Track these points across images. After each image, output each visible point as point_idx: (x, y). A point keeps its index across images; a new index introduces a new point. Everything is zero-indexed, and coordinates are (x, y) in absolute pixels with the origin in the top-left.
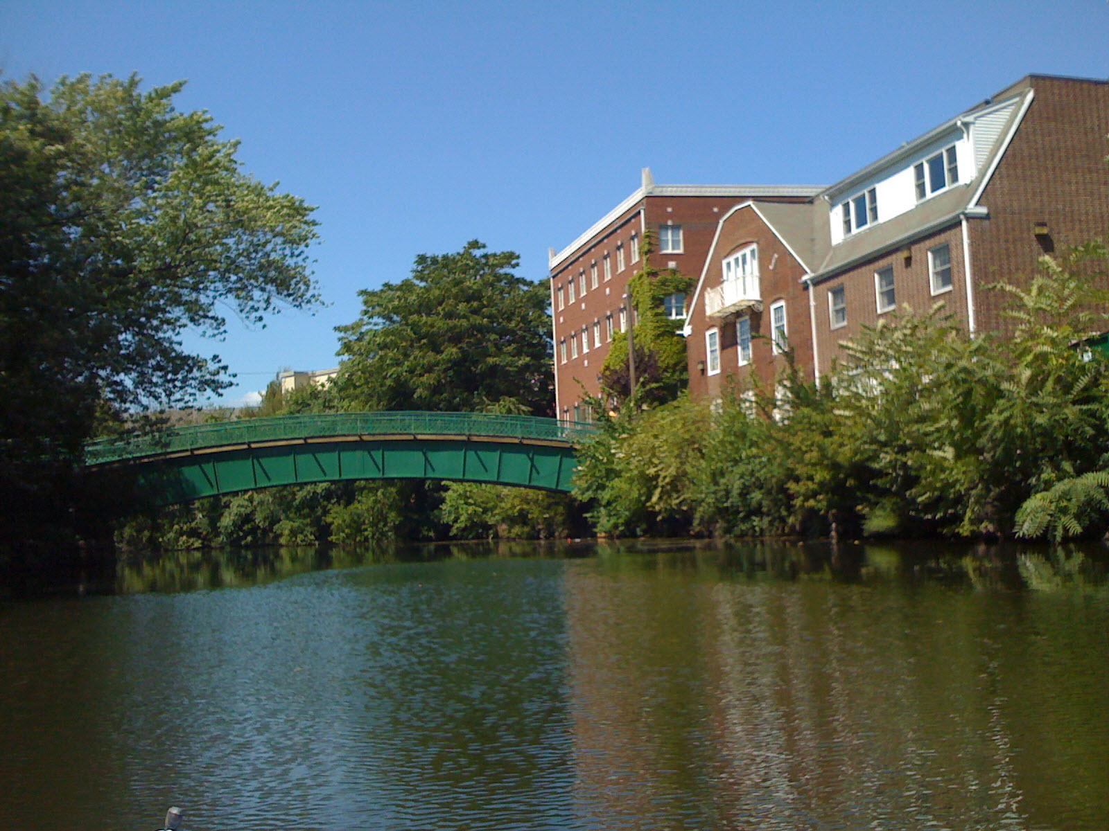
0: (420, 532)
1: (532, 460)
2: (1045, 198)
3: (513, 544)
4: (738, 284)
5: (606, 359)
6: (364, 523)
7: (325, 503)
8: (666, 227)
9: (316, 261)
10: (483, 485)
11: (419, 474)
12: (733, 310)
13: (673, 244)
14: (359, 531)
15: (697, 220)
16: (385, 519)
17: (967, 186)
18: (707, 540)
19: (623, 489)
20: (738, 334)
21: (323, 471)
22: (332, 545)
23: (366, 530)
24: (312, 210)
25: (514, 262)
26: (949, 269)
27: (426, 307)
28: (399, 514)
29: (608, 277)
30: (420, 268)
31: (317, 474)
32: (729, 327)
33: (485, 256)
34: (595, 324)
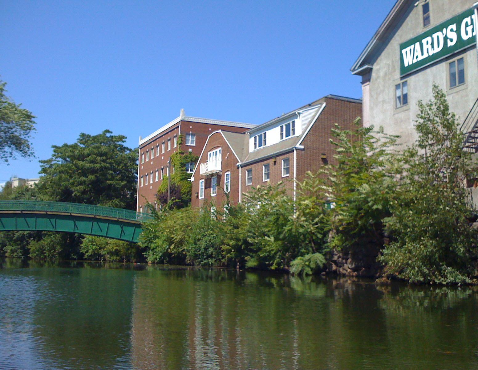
0: (71, 256)
1: (122, 228)
2: (326, 145)
3: (111, 264)
4: (212, 164)
5: (160, 186)
6: (45, 250)
7: (28, 239)
8: (189, 134)
9: (34, 138)
10: (101, 237)
11: (72, 231)
12: (210, 173)
13: (191, 142)
14: (43, 253)
15: (201, 133)
16: (54, 249)
17: (298, 137)
18: (191, 267)
19: (160, 243)
20: (212, 183)
21: (28, 226)
22: (30, 258)
23: (45, 253)
24: (34, 117)
25: (124, 140)
26: (289, 168)
27: (82, 157)
28: (61, 247)
29: (163, 152)
30: (81, 138)
31: (24, 227)
32: (209, 179)
33: (112, 137)
34: (156, 171)
